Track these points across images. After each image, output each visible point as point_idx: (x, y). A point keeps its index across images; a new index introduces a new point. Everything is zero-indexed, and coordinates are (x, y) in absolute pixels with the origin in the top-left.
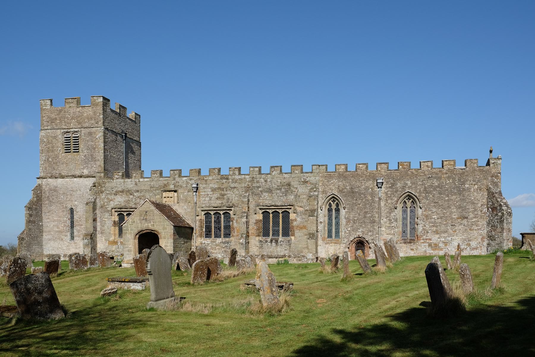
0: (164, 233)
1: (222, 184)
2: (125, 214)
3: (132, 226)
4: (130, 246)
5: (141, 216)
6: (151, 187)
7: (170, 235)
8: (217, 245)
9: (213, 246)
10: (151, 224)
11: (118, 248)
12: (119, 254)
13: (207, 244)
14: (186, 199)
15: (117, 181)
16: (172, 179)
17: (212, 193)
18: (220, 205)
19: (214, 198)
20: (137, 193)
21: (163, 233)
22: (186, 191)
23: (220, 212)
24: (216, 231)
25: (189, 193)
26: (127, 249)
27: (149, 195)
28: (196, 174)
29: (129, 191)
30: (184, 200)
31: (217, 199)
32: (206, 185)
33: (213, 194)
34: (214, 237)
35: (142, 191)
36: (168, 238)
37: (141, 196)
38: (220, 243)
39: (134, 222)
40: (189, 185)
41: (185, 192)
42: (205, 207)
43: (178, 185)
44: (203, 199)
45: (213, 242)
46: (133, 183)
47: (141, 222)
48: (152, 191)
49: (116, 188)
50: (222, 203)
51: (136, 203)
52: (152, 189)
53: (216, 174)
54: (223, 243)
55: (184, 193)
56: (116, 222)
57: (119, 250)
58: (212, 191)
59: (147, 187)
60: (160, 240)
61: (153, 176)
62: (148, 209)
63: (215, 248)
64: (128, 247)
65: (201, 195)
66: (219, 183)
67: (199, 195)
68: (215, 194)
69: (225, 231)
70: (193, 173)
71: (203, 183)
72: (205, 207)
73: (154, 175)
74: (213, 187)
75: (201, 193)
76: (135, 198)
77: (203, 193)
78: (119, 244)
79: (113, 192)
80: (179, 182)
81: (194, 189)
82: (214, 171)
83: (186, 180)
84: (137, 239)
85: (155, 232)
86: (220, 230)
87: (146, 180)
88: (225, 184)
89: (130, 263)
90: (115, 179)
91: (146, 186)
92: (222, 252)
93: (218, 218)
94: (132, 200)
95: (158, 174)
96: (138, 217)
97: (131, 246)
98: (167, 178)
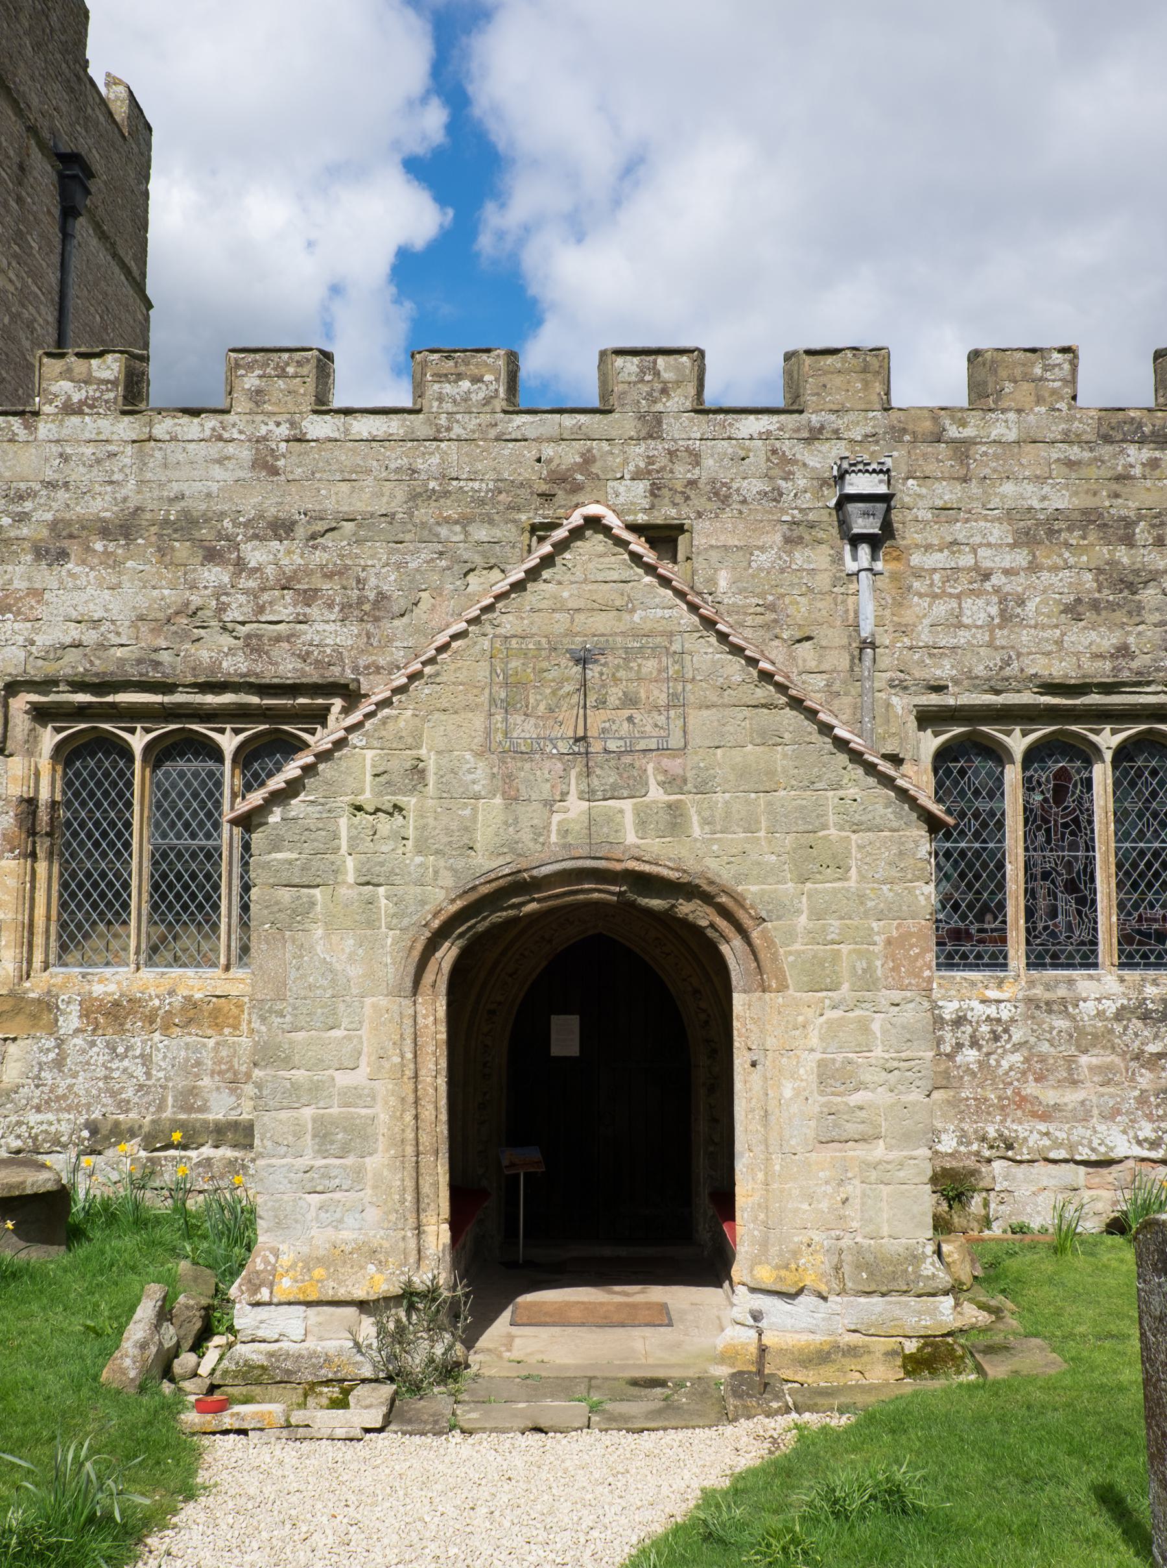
0: (817, 915)
1: (1115, 487)
2: (138, 741)
3: (384, 824)
4: (343, 1079)
5: (508, 707)
6: (414, 497)
7: (889, 942)
8: (1083, 1039)
9: (1045, 1047)
10: (637, 812)
11: (59, 1063)
12: (64, 1128)
13: (985, 1028)
14: (772, 608)
15: (65, 432)
16: (624, 423)
17: (1021, 558)
18: (1108, 665)
19: (1045, 602)
20: (275, 544)
21: (803, 920)
22: (766, 539)
23: (1093, 737)
24: (1042, 903)
25: (800, 557)
26: (308, 1113)
27: (399, 566)
28: (866, 385)
29: (187, 525)
30: (749, 621)
31: (1073, 611)
32: (958, 487)
33: (1034, 568)
34: (1029, 965)
35: (320, 526)
36: (867, 982)
37: (310, 573)
38: (1118, 1017)
39: (417, 772)
40: (802, 483)
41: (762, 549)
42: (956, 682)
43: (692, 483)
44: (941, 609)
45: (1050, 1011)
46: (231, 449)
47: (509, 777)
48: (426, 534)
49: (62, 495)
50: (1123, 651)
51: (259, 637)
52: (424, 513)
53: (1054, 392)
54: (1145, 1017)
55: (748, 550)
56: (43, 816)
57: (63, 1085)
58: (1025, 539)
59: (374, 495)
60: (739, 1001)
61: (440, 399)
62: (602, 623)
63: (1070, 1060)
64: (316, 1090)
65: (918, 573)
66: (1085, 472)
67: (895, 577)
68: (1054, 569)
69: (1136, 906)
70: (838, 380)
71: (931, 468)
72: (956, 682)
73: (448, 388)
74: (1030, 509)
75: (916, 559)
76: (246, 592)
77: (938, 559)
78: (71, 1021)
79: (25, 531)
80: (696, 458)
81: (866, 514)
82: (1038, 371)
83: (766, 436)
84: (443, 987)
85: (686, 908)
86: (1081, 901)
87: (363, 426)
88: (1149, 483)
89: (360, 1294)
90: (47, 409)
91: (370, 481)
92: (1142, 1100)
93: (1060, 793)
94: (222, 609)
95: (487, 378)
96: (478, 721)
97: (358, 1078)
98: (583, 418)
